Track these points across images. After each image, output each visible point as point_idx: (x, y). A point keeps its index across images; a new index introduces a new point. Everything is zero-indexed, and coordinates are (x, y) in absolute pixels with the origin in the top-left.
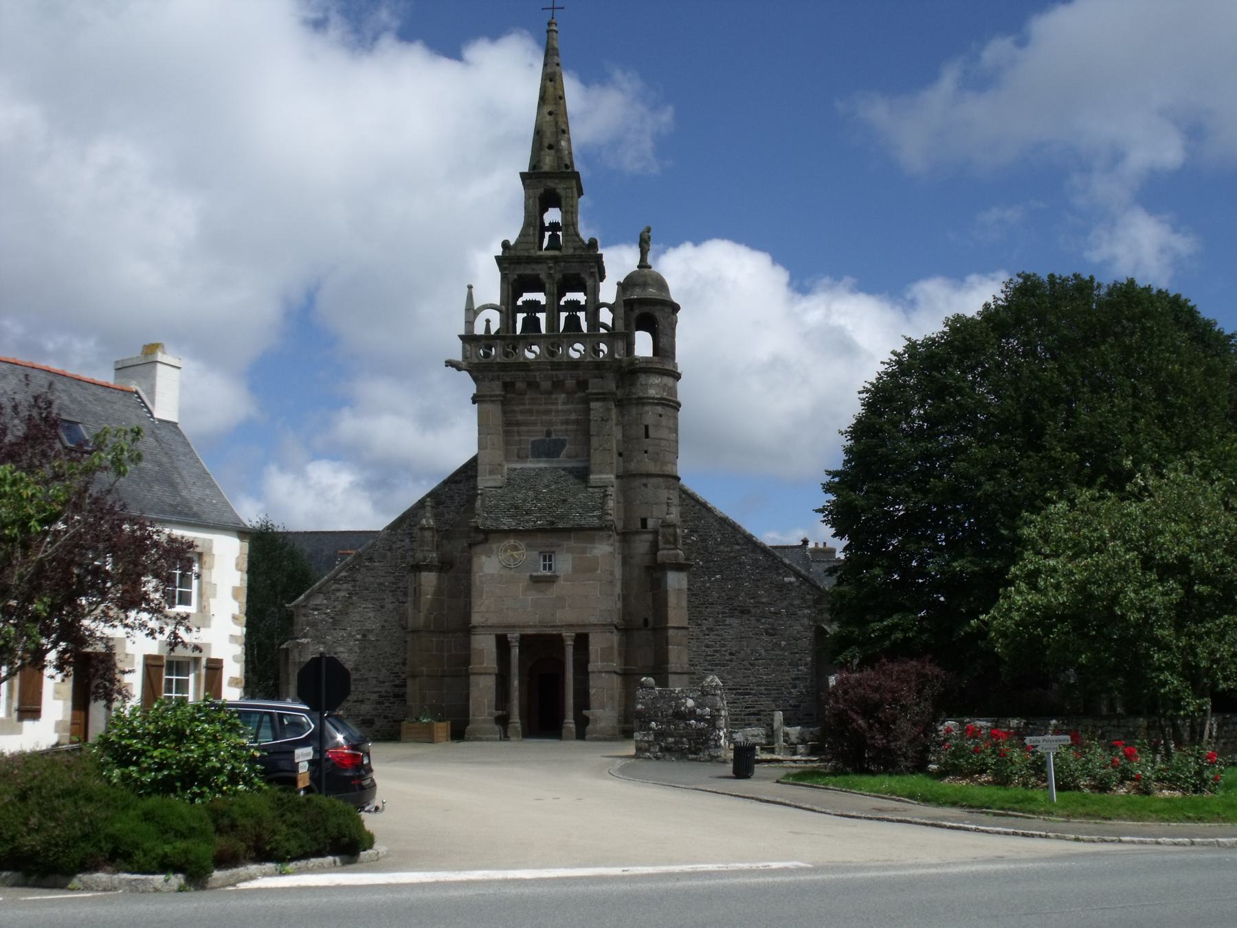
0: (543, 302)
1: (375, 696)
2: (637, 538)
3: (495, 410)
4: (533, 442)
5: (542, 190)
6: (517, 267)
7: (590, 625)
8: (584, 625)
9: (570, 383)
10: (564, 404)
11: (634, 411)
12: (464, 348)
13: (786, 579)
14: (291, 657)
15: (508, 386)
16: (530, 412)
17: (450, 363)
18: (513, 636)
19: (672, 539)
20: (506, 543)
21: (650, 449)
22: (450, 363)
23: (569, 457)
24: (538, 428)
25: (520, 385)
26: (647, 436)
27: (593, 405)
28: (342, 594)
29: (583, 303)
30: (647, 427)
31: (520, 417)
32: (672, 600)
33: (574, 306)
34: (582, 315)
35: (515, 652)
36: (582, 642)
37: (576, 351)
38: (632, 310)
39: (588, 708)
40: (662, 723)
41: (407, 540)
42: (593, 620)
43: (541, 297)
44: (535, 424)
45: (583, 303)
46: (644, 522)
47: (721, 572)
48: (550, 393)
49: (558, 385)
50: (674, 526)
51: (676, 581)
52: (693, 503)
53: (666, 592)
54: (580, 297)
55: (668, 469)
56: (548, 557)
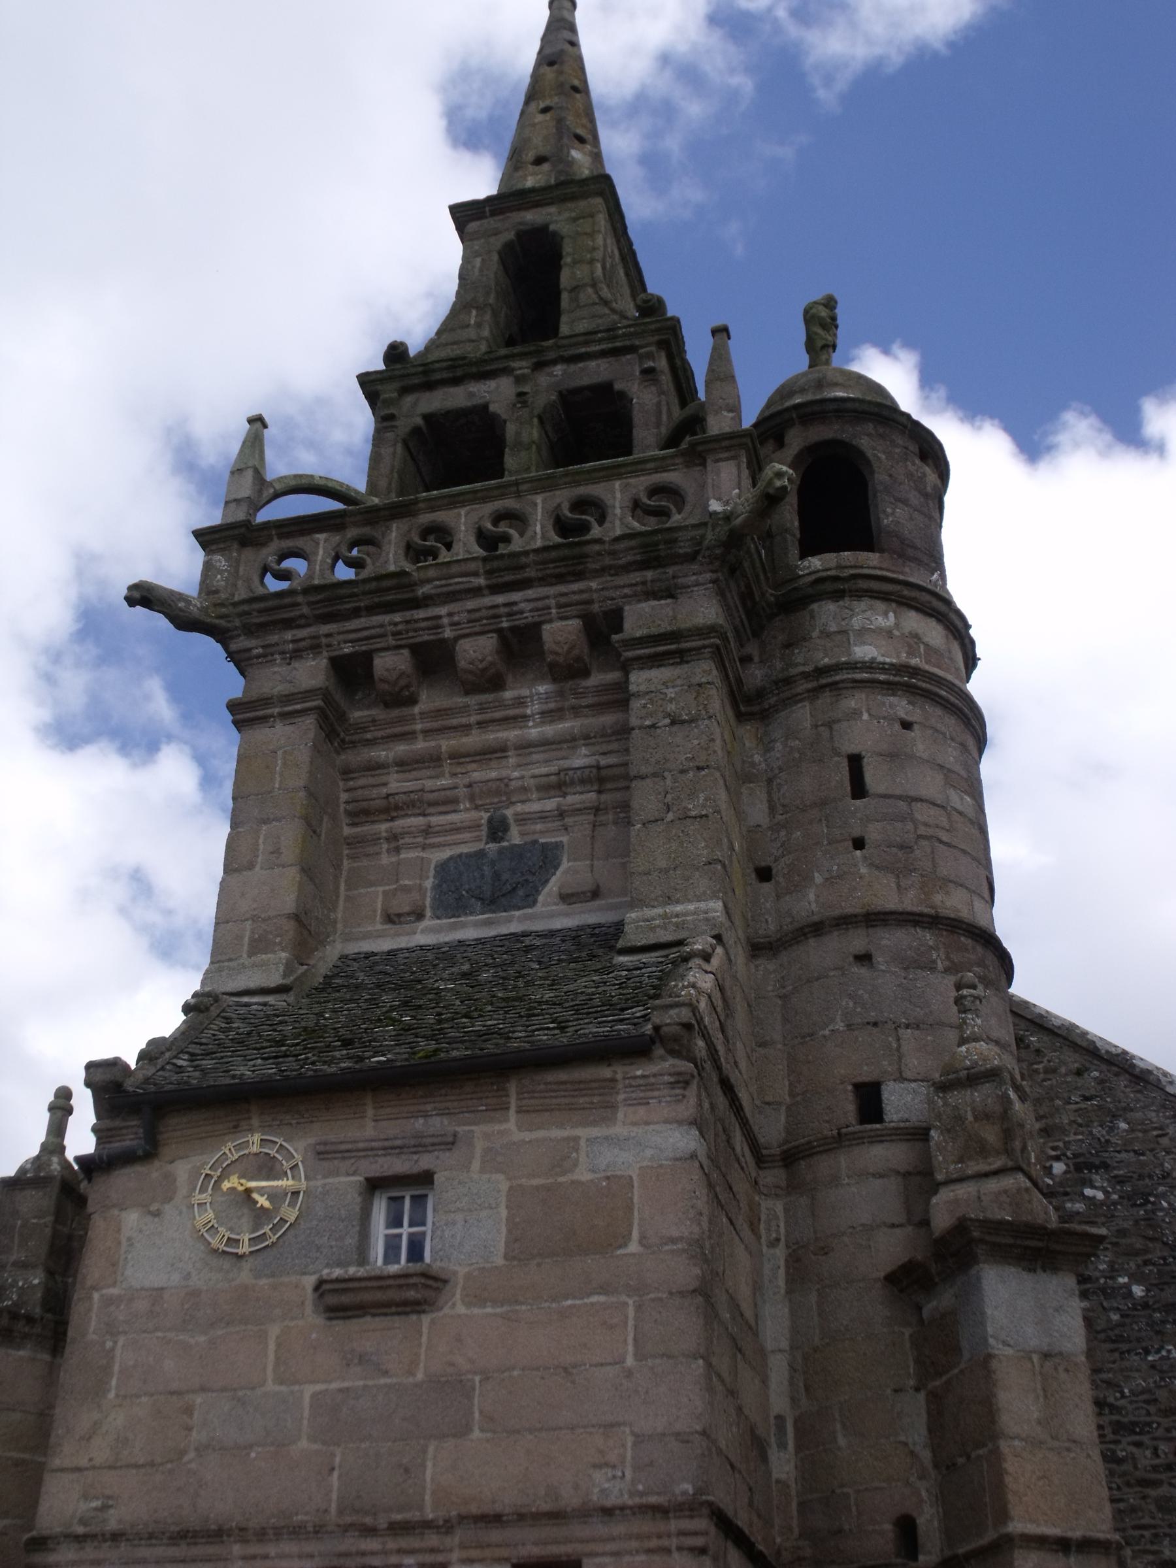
2: (843, 1160)
3: (293, 739)
4: (442, 867)
5: (510, 236)
7: (585, 1513)
8: (556, 1516)
9: (562, 633)
10: (549, 716)
11: (803, 715)
12: (208, 567)
15: (352, 673)
16: (434, 760)
19: (990, 1134)
20: (229, 1150)
21: (873, 833)
23: (566, 898)
24: (463, 816)
25: (391, 664)
26: (859, 789)
27: (639, 679)
30: (855, 762)
31: (396, 783)
32: (1017, 1405)
42: (610, 1487)
44: (449, 803)
46: (869, 1100)
48: (496, 683)
49: (520, 646)
50: (993, 1075)
51: (1023, 1316)
52: (1073, 1061)
53: (986, 1361)
55: (953, 903)
56: (407, 1188)
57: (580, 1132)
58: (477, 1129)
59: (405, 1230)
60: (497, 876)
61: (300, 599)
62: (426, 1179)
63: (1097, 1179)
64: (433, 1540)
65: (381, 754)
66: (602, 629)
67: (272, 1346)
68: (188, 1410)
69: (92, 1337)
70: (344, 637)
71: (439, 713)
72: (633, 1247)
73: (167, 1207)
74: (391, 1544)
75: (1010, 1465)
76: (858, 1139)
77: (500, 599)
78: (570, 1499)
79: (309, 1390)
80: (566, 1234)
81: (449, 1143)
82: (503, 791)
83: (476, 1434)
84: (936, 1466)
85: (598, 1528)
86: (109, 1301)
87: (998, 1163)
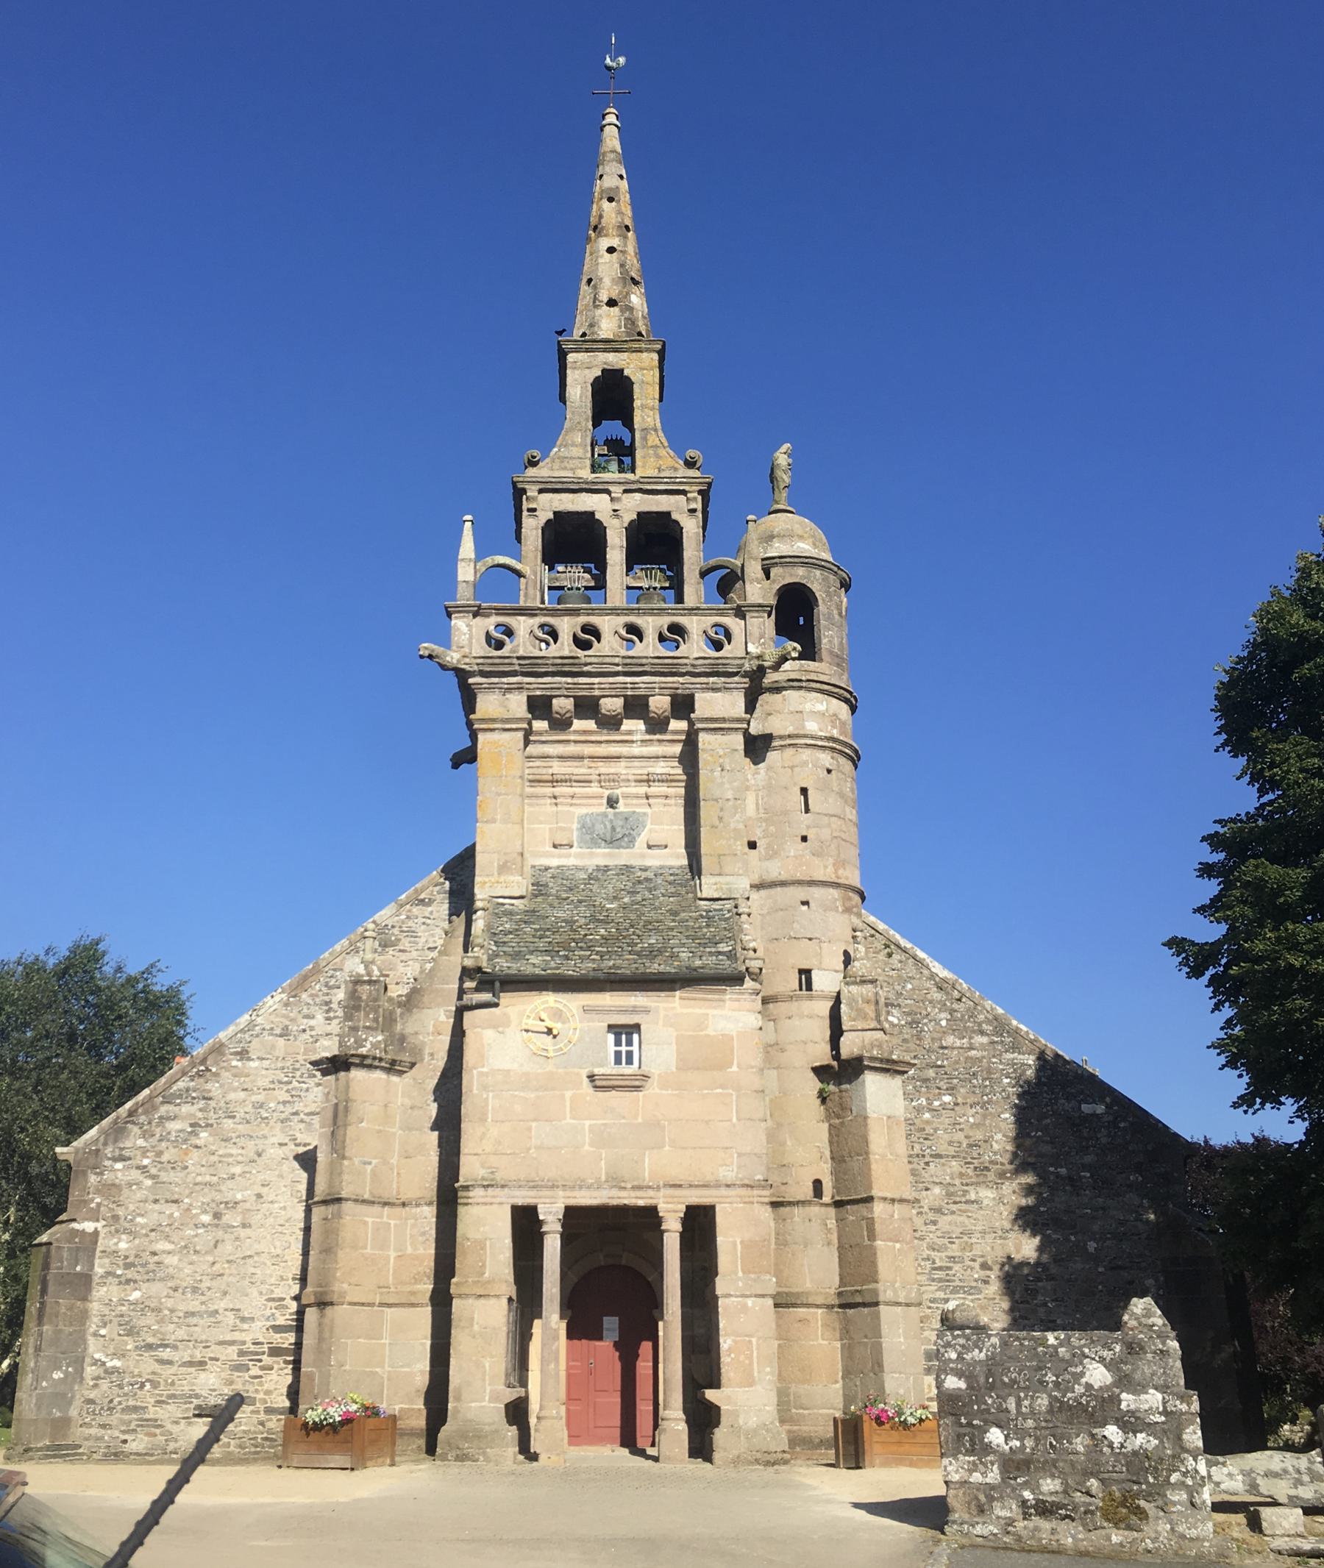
1: (232, 1352)
9: (660, 703)
13: (1086, 1108)
14: (54, 1265)
15: (539, 706)
24: (594, 789)
28: (173, 1126)
35: (552, 1246)
36: (700, 1223)
39: (716, 1384)
40: (1022, 1434)
41: (320, 1017)
42: (728, 1174)
47: (951, 1090)
57: (711, 1012)
58: (661, 1005)
59: (624, 1048)
60: (613, 829)
61: (515, 661)
62: (637, 1027)
63: (895, 1011)
64: (651, 1193)
66: (683, 705)
67: (568, 1104)
68: (529, 1129)
69: (475, 1091)
70: (539, 686)
71: (585, 732)
72: (735, 1068)
73: (507, 1030)
74: (633, 1194)
75: (874, 1166)
76: (799, 998)
77: (629, 679)
78: (709, 1178)
79: (587, 1123)
80: (705, 1058)
81: (647, 1011)
82: (614, 780)
83: (667, 1148)
84: (832, 1158)
85: (723, 1191)
86: (481, 1074)
87: (872, 1026)
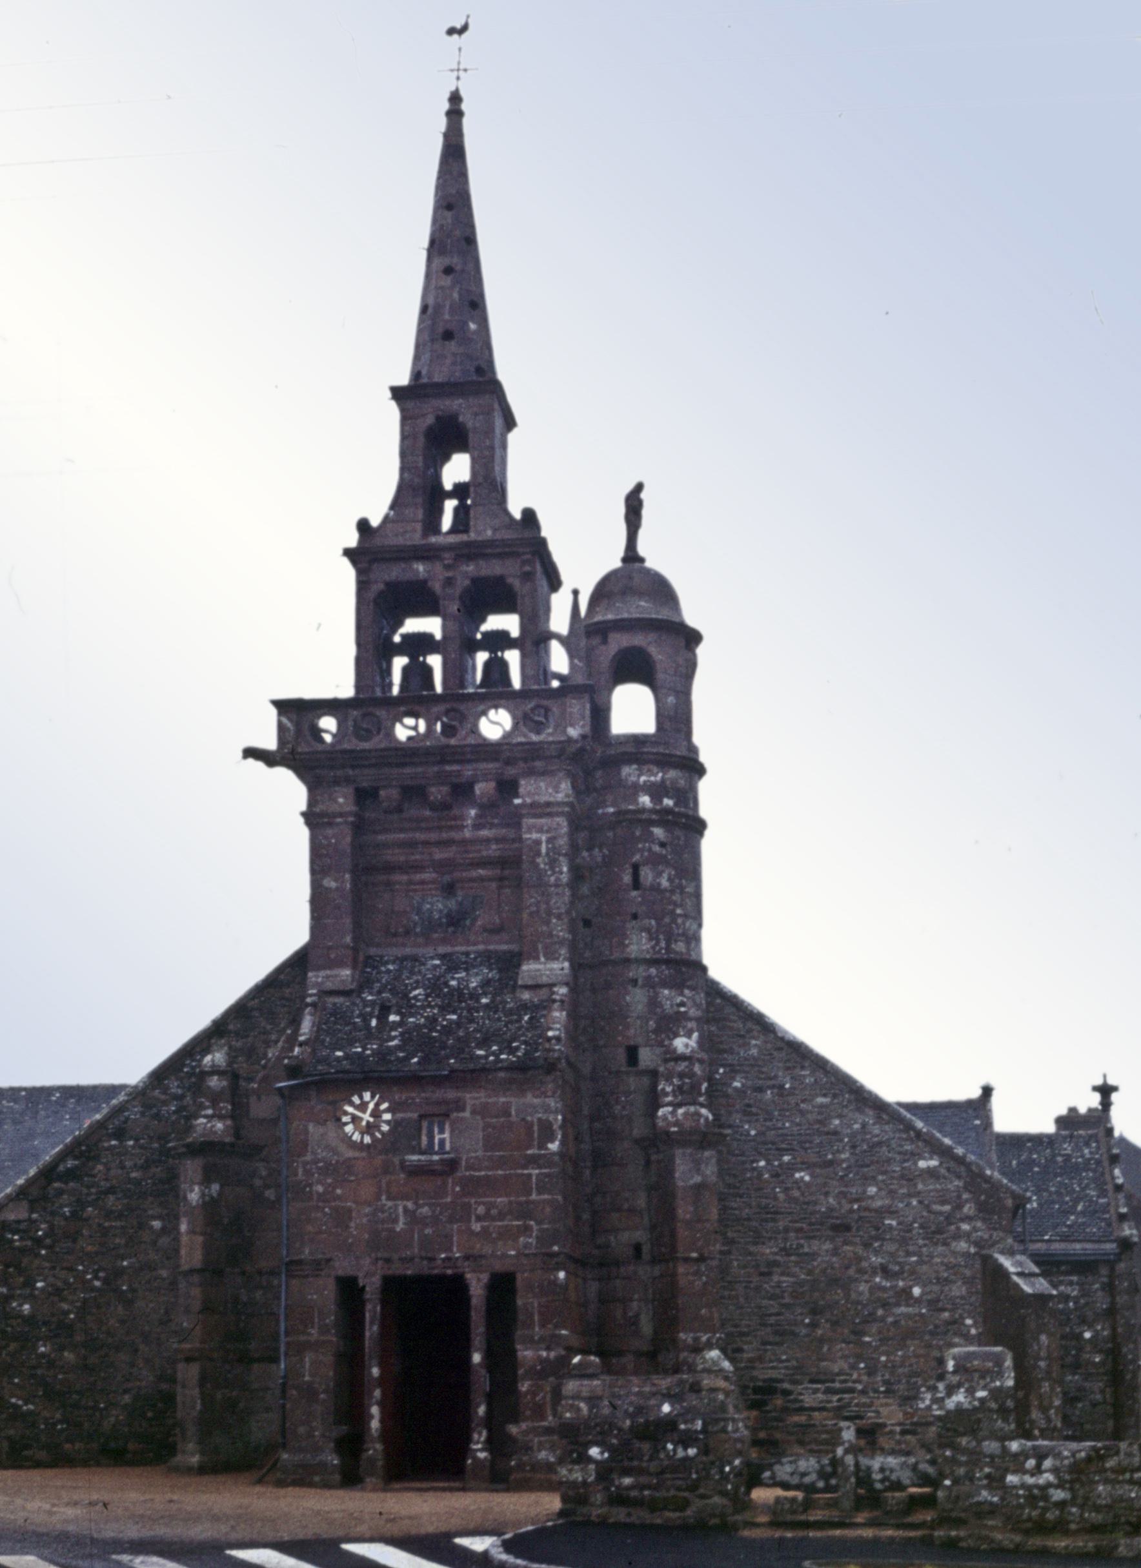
0: (515, 633)
5: (430, 420)
6: (390, 572)
17: (251, 753)
18: (372, 1285)
22: (251, 753)
29: (438, 636)
33: (500, 640)
34: (513, 657)
35: (372, 1310)
37: (495, 725)
38: (605, 641)
43: (432, 625)
44: (418, 868)
45: (438, 636)
54: (508, 623)
65: (381, 838)
70: (366, 778)
